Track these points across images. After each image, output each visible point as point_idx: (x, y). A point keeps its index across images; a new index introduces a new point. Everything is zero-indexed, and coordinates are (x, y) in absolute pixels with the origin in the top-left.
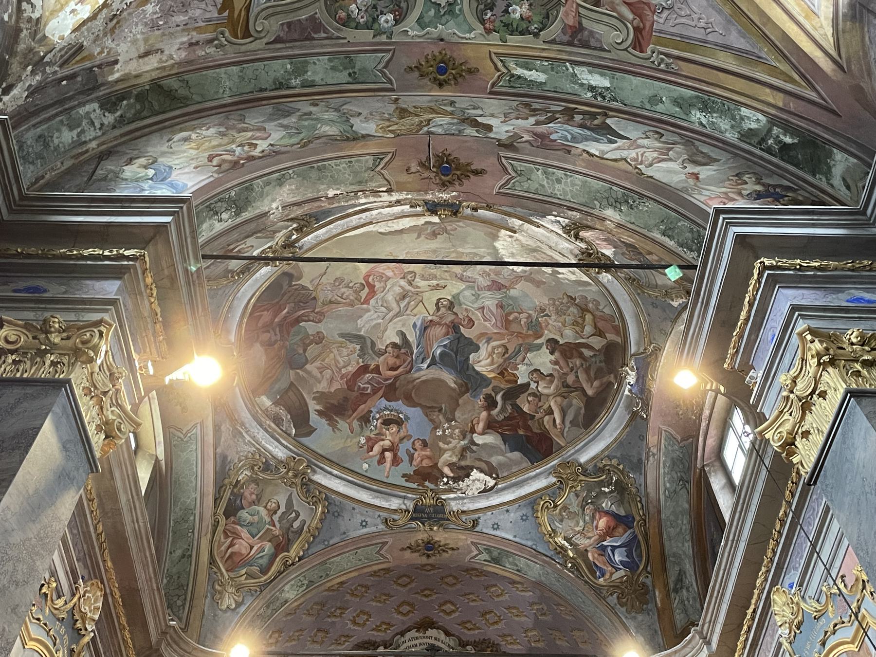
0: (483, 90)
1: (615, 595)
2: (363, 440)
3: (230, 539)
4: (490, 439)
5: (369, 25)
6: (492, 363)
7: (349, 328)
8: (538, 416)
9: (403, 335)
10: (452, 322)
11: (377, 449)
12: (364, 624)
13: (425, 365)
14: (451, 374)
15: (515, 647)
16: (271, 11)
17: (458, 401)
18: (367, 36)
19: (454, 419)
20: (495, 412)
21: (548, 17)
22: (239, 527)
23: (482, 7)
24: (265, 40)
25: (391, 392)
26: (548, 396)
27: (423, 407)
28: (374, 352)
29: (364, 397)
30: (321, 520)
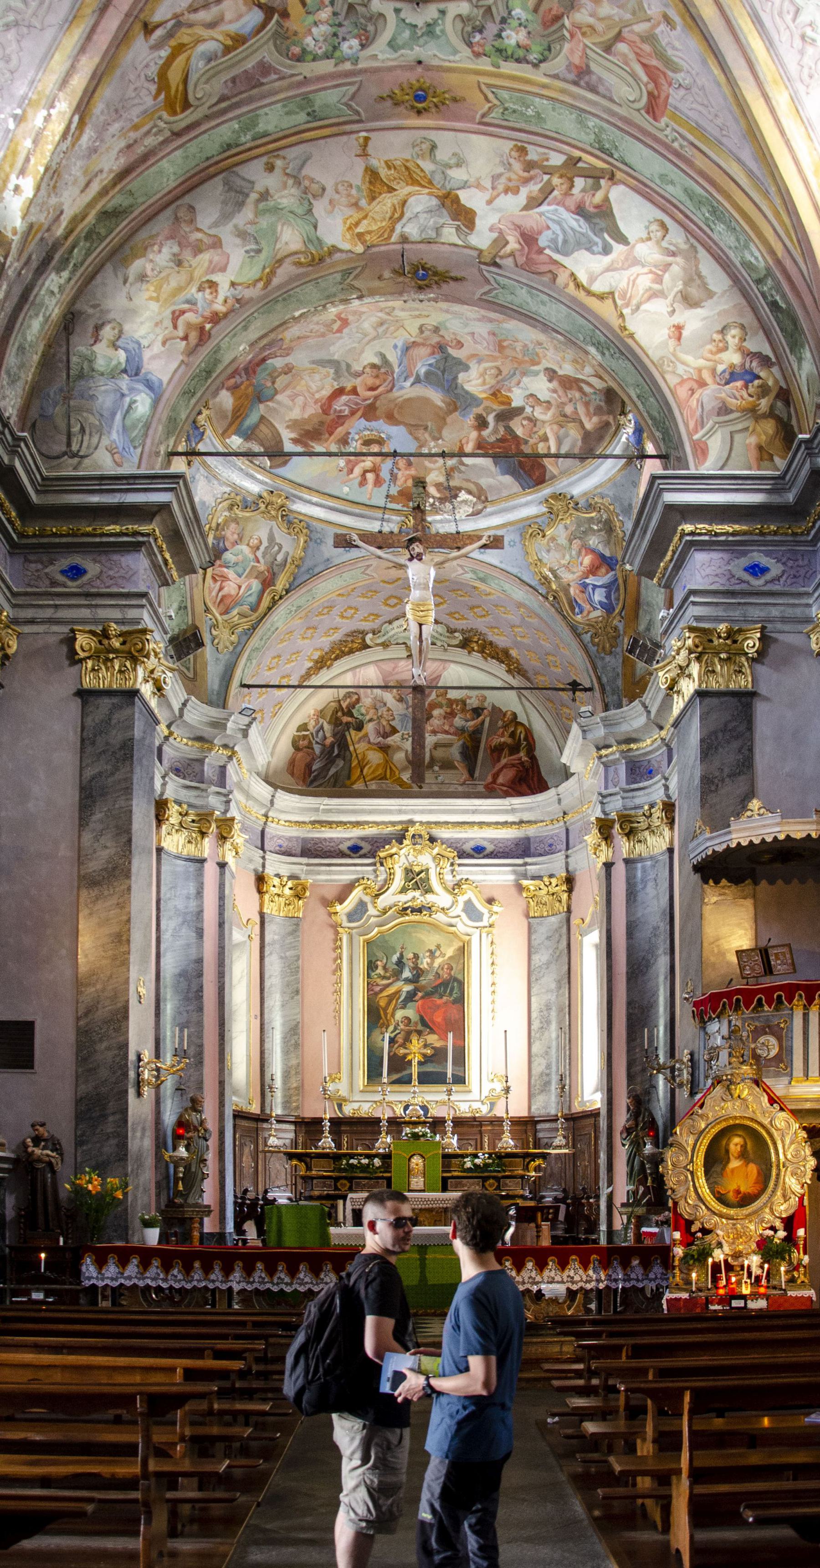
0: (472, 120)
1: (589, 634)
3: (219, 583)
5: (329, 54)
6: (484, 383)
7: (322, 355)
8: (532, 441)
9: (383, 356)
10: (438, 343)
11: (357, 471)
12: (352, 617)
13: (408, 384)
14: (437, 391)
15: (502, 638)
16: (211, 72)
17: (444, 419)
18: (326, 67)
19: (440, 438)
20: (485, 433)
21: (549, 49)
22: (225, 570)
23: (469, 29)
24: (208, 104)
25: (370, 412)
26: (544, 422)
27: (406, 425)
28: (350, 374)
29: (340, 419)
30: (305, 549)
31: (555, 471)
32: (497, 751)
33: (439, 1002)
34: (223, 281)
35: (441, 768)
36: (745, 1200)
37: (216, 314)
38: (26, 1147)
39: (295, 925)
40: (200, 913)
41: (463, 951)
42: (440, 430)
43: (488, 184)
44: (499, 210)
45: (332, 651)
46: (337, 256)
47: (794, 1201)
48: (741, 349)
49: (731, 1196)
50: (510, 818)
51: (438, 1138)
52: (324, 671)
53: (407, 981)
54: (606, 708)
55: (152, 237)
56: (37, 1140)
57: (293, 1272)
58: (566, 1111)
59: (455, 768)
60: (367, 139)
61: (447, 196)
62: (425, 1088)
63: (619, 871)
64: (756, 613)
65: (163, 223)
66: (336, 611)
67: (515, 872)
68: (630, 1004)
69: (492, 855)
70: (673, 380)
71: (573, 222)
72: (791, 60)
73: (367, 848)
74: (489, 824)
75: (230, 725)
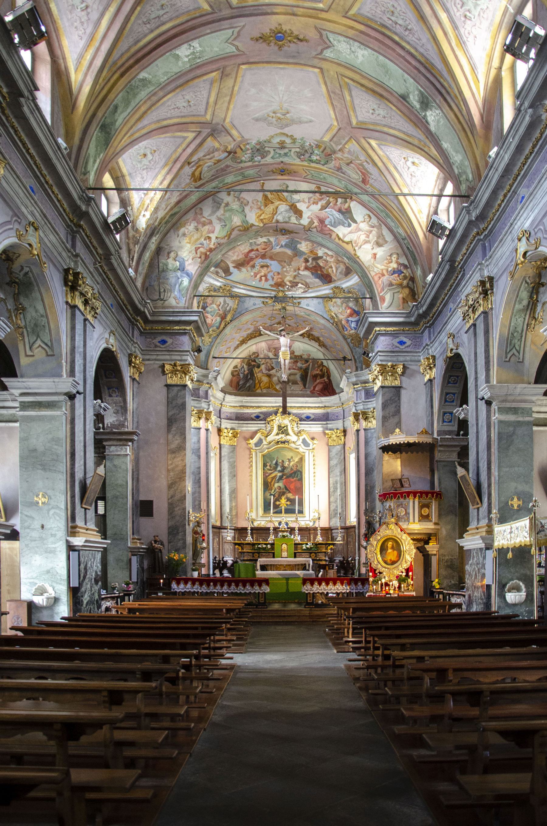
2: (252, 274)
4: (307, 273)
11: (258, 276)
20: (308, 264)
25: (263, 257)
29: (252, 259)
31: (336, 279)
32: (315, 377)
33: (292, 480)
34: (213, 236)
35: (292, 384)
36: (393, 563)
37: (211, 249)
38: (152, 544)
39: (233, 448)
40: (199, 449)
41: (301, 460)
42: (291, 262)
43: (307, 200)
44: (311, 210)
45: (247, 337)
46: (254, 227)
47: (409, 563)
48: (397, 262)
49: (389, 561)
50: (321, 405)
51: (292, 537)
52: (244, 345)
53: (279, 471)
54: (357, 370)
55: (187, 220)
56: (156, 542)
57: (244, 586)
58: (343, 525)
59: (298, 384)
60: (263, 183)
61: (292, 205)
62: (287, 515)
63: (362, 433)
64: (401, 359)
65: (191, 215)
66: (249, 323)
67: (322, 427)
68: (366, 485)
69: (313, 420)
70: (373, 274)
71: (337, 215)
72: (408, 181)
73: (262, 416)
74: (312, 407)
75: (210, 376)
